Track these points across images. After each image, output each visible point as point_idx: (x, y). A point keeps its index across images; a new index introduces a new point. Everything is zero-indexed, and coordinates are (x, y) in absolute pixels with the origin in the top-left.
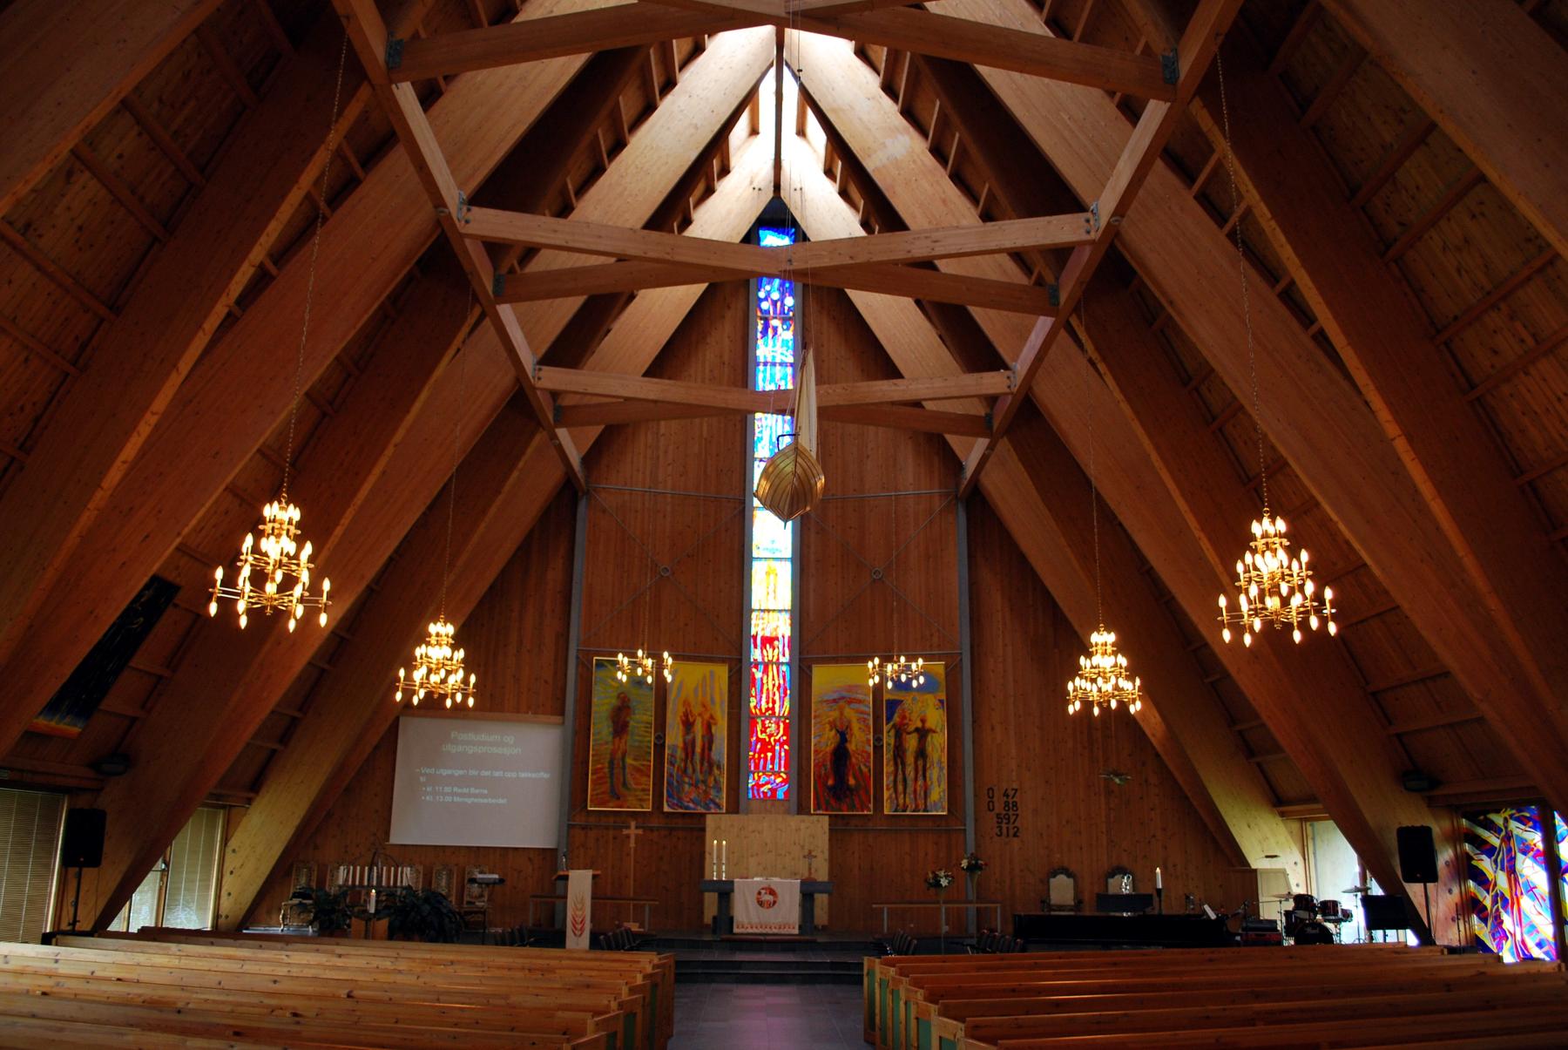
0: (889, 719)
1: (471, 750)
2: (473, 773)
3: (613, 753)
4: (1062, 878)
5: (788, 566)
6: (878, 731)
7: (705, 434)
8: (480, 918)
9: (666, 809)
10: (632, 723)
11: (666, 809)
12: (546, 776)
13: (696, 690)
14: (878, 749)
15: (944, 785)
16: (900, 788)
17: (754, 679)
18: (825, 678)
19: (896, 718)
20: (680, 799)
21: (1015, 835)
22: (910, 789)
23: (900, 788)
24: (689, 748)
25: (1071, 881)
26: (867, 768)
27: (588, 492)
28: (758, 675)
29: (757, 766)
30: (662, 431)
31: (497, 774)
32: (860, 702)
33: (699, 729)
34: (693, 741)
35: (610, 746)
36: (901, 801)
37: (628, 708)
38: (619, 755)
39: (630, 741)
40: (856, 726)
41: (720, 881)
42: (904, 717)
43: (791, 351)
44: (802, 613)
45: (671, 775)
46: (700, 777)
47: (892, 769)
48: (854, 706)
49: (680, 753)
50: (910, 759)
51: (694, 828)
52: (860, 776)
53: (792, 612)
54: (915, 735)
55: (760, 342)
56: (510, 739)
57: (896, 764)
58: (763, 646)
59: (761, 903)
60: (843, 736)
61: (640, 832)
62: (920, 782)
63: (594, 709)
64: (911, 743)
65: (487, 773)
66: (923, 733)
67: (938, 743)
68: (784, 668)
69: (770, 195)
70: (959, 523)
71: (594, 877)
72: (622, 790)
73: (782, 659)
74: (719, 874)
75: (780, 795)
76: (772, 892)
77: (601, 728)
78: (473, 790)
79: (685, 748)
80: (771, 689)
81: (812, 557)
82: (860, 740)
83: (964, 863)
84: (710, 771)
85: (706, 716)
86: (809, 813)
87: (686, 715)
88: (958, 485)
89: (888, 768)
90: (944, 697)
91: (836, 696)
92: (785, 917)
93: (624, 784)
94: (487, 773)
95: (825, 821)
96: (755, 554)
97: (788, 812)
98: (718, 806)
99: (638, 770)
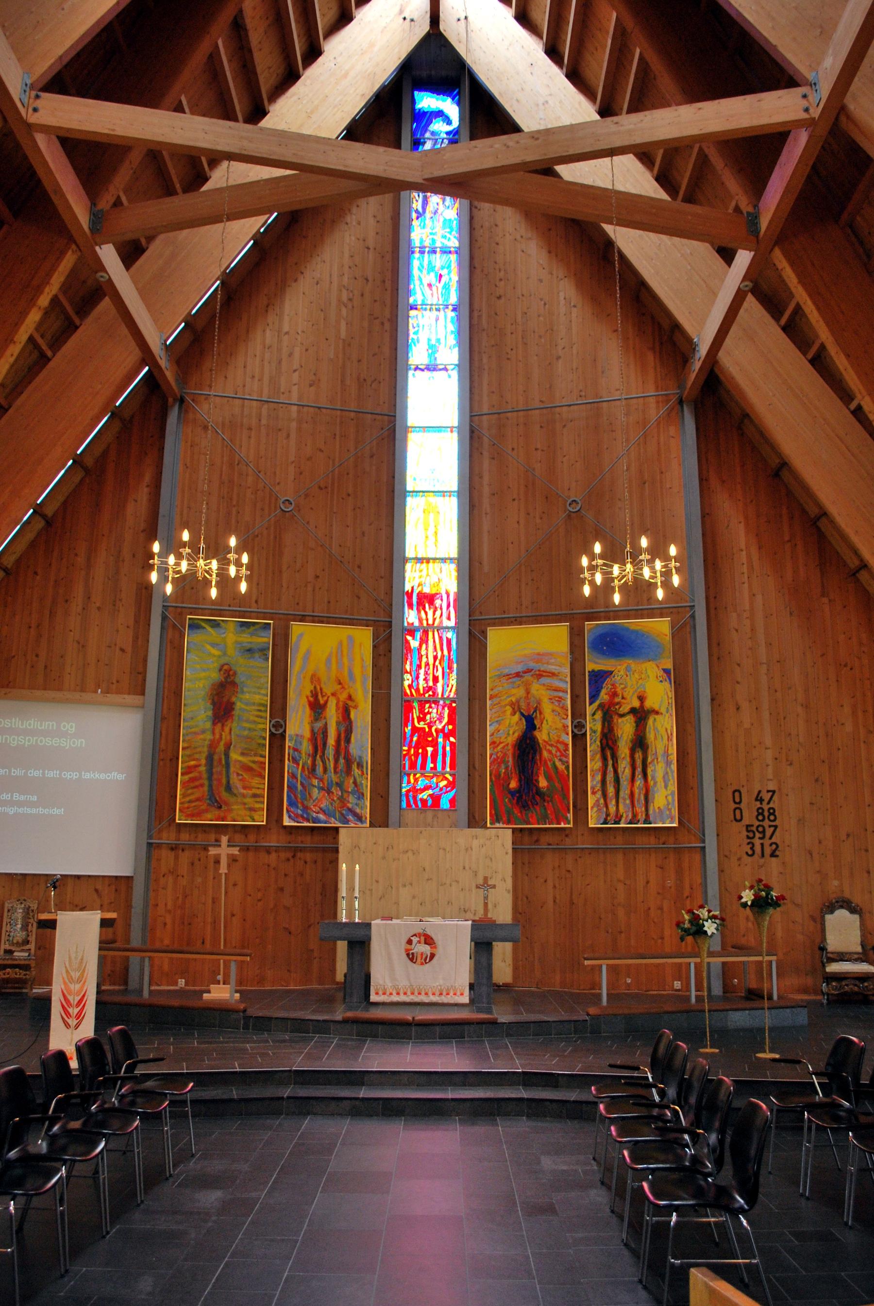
0: (594, 697)
1: (14, 741)
2: (17, 772)
3: (213, 746)
4: (842, 914)
5: (453, 502)
6: (578, 714)
7: (343, 334)
8: (18, 974)
9: (287, 822)
10: (239, 705)
11: (287, 822)
12: (118, 776)
13: (328, 660)
14: (579, 738)
15: (673, 787)
16: (611, 790)
17: (409, 649)
18: (505, 645)
19: (604, 696)
20: (306, 808)
21: (773, 855)
22: (625, 792)
23: (611, 790)
24: (318, 740)
25: (856, 917)
26: (566, 764)
27: (182, 400)
28: (414, 644)
29: (413, 766)
30: (286, 328)
31: (50, 774)
32: (553, 675)
33: (332, 714)
34: (325, 731)
35: (209, 736)
36: (612, 809)
37: (234, 684)
38: (221, 747)
39: (236, 728)
40: (547, 708)
41: (351, 925)
42: (614, 694)
43: (455, 233)
44: (471, 563)
45: (293, 776)
46: (335, 778)
47: (598, 764)
48: (543, 680)
49: (306, 747)
50: (624, 750)
51: (323, 845)
52: (555, 776)
53: (459, 561)
54: (630, 719)
55: (415, 223)
56: (70, 727)
57: (604, 759)
58: (421, 605)
59: (412, 957)
60: (531, 723)
61: (235, 851)
62: (639, 782)
63: (185, 685)
64: (626, 728)
65: (37, 773)
66: (641, 715)
67: (663, 730)
68: (450, 635)
69: (425, 27)
70: (682, 443)
71: (105, 923)
72: (225, 795)
73: (446, 623)
74: (350, 914)
75: (445, 803)
76: (428, 940)
77: (196, 711)
78: (16, 797)
79: (313, 739)
80: (432, 665)
81: (486, 490)
82: (554, 728)
83: (748, 896)
84: (348, 771)
85: (343, 697)
86: (485, 826)
87: (315, 694)
88: (681, 386)
89: (593, 764)
90: (669, 665)
91: (520, 668)
92: (449, 980)
93: (228, 788)
94: (37, 773)
95: (507, 836)
96: (409, 488)
97: (454, 825)
98: (359, 818)
99: (247, 769)
